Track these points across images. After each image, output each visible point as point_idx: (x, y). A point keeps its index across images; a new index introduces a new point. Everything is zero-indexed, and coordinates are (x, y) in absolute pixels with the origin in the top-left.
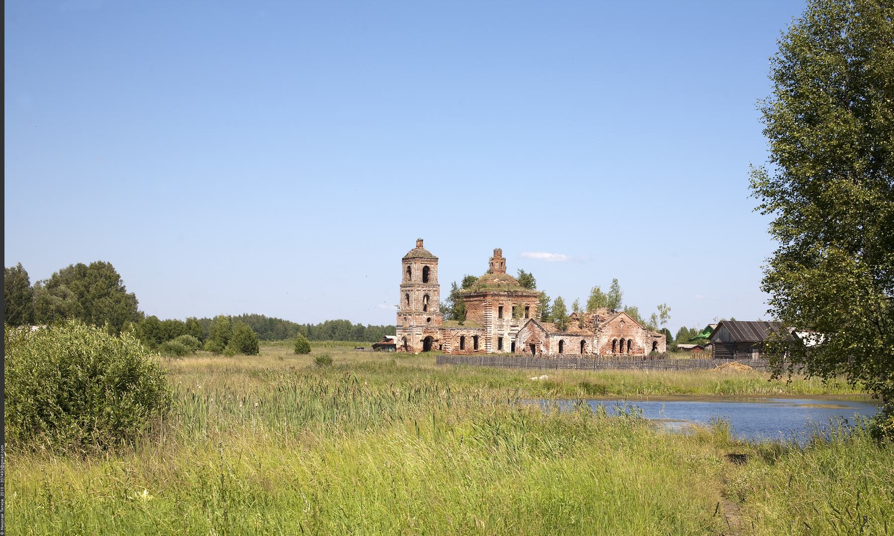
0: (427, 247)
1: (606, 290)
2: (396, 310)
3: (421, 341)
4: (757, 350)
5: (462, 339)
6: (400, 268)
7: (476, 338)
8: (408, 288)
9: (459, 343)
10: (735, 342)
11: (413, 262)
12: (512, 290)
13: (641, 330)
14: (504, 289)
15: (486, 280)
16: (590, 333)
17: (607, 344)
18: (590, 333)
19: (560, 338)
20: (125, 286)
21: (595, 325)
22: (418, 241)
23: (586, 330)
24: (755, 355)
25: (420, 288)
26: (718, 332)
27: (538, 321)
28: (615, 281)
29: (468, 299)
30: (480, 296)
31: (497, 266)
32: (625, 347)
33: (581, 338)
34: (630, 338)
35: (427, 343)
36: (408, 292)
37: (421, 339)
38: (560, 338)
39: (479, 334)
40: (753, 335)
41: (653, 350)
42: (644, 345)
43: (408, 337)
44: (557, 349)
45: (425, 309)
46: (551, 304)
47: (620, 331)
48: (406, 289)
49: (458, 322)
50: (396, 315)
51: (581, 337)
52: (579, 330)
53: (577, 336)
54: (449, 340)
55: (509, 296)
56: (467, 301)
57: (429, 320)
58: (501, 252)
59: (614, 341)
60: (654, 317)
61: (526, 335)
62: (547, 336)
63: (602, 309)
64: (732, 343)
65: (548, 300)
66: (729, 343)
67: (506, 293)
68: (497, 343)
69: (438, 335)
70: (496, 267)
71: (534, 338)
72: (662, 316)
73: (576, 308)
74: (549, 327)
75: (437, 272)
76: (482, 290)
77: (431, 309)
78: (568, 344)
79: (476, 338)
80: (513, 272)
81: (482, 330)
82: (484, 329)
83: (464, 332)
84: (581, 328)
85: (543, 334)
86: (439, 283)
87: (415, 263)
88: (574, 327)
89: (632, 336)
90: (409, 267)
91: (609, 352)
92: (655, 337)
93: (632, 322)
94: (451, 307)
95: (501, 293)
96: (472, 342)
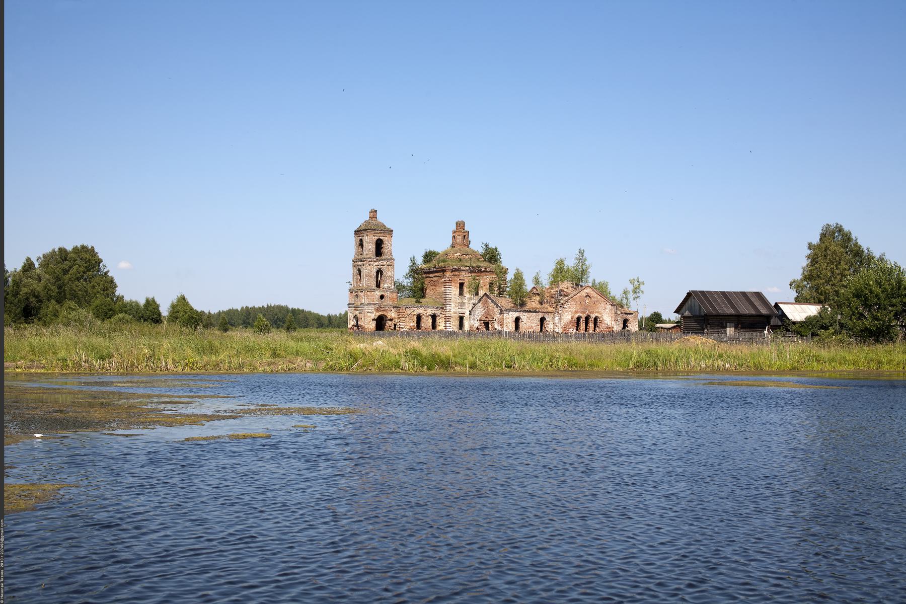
0: (381, 218)
1: (570, 263)
2: (348, 286)
3: (373, 320)
4: (732, 325)
5: (419, 318)
6: (352, 241)
7: (434, 317)
8: (360, 263)
9: (416, 322)
10: (706, 315)
11: (365, 235)
12: (474, 265)
13: (609, 307)
14: (466, 264)
15: (446, 254)
16: (551, 309)
17: (571, 322)
18: (551, 309)
19: (516, 314)
20: (108, 271)
21: (557, 301)
22: (372, 211)
23: (547, 306)
24: (730, 331)
25: (372, 263)
26: (687, 304)
27: (492, 296)
28: (581, 252)
29: (428, 275)
30: (440, 271)
31: (459, 239)
32: (591, 325)
33: (540, 315)
34: (596, 315)
35: (381, 323)
36: (360, 267)
37: (373, 317)
38: (516, 314)
39: (438, 312)
40: (727, 307)
41: (624, 328)
42: (613, 323)
43: (359, 316)
44: (512, 327)
45: (378, 286)
46: (510, 277)
47: (586, 307)
48: (358, 262)
49: (415, 300)
50: (348, 293)
51: (541, 314)
52: (539, 306)
53: (536, 312)
54: (404, 319)
55: (471, 272)
56: (426, 277)
57: (382, 297)
58: (464, 224)
59: (579, 319)
60: (625, 293)
61: (480, 312)
62: (501, 313)
63: (566, 282)
64: (702, 316)
65: (506, 271)
66: (700, 316)
67: (467, 268)
68: (457, 323)
69: (392, 314)
70: (458, 241)
71: (488, 314)
72: (635, 292)
73: (537, 281)
74: (505, 302)
75: (391, 245)
76: (441, 264)
77: (384, 285)
78: (525, 322)
79: (434, 317)
80: (477, 246)
81: (441, 308)
82: (443, 308)
83: (420, 311)
84: (541, 303)
85: (497, 310)
86: (393, 257)
87: (367, 235)
88: (533, 303)
89: (598, 312)
90: (361, 240)
91: (573, 330)
92: (626, 314)
93: (599, 297)
94: (409, 285)
95: (462, 268)
96: (430, 321)
